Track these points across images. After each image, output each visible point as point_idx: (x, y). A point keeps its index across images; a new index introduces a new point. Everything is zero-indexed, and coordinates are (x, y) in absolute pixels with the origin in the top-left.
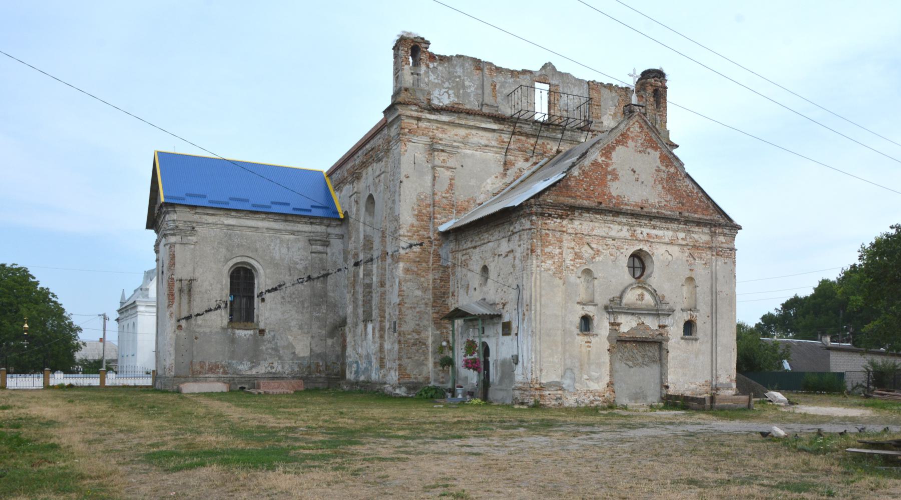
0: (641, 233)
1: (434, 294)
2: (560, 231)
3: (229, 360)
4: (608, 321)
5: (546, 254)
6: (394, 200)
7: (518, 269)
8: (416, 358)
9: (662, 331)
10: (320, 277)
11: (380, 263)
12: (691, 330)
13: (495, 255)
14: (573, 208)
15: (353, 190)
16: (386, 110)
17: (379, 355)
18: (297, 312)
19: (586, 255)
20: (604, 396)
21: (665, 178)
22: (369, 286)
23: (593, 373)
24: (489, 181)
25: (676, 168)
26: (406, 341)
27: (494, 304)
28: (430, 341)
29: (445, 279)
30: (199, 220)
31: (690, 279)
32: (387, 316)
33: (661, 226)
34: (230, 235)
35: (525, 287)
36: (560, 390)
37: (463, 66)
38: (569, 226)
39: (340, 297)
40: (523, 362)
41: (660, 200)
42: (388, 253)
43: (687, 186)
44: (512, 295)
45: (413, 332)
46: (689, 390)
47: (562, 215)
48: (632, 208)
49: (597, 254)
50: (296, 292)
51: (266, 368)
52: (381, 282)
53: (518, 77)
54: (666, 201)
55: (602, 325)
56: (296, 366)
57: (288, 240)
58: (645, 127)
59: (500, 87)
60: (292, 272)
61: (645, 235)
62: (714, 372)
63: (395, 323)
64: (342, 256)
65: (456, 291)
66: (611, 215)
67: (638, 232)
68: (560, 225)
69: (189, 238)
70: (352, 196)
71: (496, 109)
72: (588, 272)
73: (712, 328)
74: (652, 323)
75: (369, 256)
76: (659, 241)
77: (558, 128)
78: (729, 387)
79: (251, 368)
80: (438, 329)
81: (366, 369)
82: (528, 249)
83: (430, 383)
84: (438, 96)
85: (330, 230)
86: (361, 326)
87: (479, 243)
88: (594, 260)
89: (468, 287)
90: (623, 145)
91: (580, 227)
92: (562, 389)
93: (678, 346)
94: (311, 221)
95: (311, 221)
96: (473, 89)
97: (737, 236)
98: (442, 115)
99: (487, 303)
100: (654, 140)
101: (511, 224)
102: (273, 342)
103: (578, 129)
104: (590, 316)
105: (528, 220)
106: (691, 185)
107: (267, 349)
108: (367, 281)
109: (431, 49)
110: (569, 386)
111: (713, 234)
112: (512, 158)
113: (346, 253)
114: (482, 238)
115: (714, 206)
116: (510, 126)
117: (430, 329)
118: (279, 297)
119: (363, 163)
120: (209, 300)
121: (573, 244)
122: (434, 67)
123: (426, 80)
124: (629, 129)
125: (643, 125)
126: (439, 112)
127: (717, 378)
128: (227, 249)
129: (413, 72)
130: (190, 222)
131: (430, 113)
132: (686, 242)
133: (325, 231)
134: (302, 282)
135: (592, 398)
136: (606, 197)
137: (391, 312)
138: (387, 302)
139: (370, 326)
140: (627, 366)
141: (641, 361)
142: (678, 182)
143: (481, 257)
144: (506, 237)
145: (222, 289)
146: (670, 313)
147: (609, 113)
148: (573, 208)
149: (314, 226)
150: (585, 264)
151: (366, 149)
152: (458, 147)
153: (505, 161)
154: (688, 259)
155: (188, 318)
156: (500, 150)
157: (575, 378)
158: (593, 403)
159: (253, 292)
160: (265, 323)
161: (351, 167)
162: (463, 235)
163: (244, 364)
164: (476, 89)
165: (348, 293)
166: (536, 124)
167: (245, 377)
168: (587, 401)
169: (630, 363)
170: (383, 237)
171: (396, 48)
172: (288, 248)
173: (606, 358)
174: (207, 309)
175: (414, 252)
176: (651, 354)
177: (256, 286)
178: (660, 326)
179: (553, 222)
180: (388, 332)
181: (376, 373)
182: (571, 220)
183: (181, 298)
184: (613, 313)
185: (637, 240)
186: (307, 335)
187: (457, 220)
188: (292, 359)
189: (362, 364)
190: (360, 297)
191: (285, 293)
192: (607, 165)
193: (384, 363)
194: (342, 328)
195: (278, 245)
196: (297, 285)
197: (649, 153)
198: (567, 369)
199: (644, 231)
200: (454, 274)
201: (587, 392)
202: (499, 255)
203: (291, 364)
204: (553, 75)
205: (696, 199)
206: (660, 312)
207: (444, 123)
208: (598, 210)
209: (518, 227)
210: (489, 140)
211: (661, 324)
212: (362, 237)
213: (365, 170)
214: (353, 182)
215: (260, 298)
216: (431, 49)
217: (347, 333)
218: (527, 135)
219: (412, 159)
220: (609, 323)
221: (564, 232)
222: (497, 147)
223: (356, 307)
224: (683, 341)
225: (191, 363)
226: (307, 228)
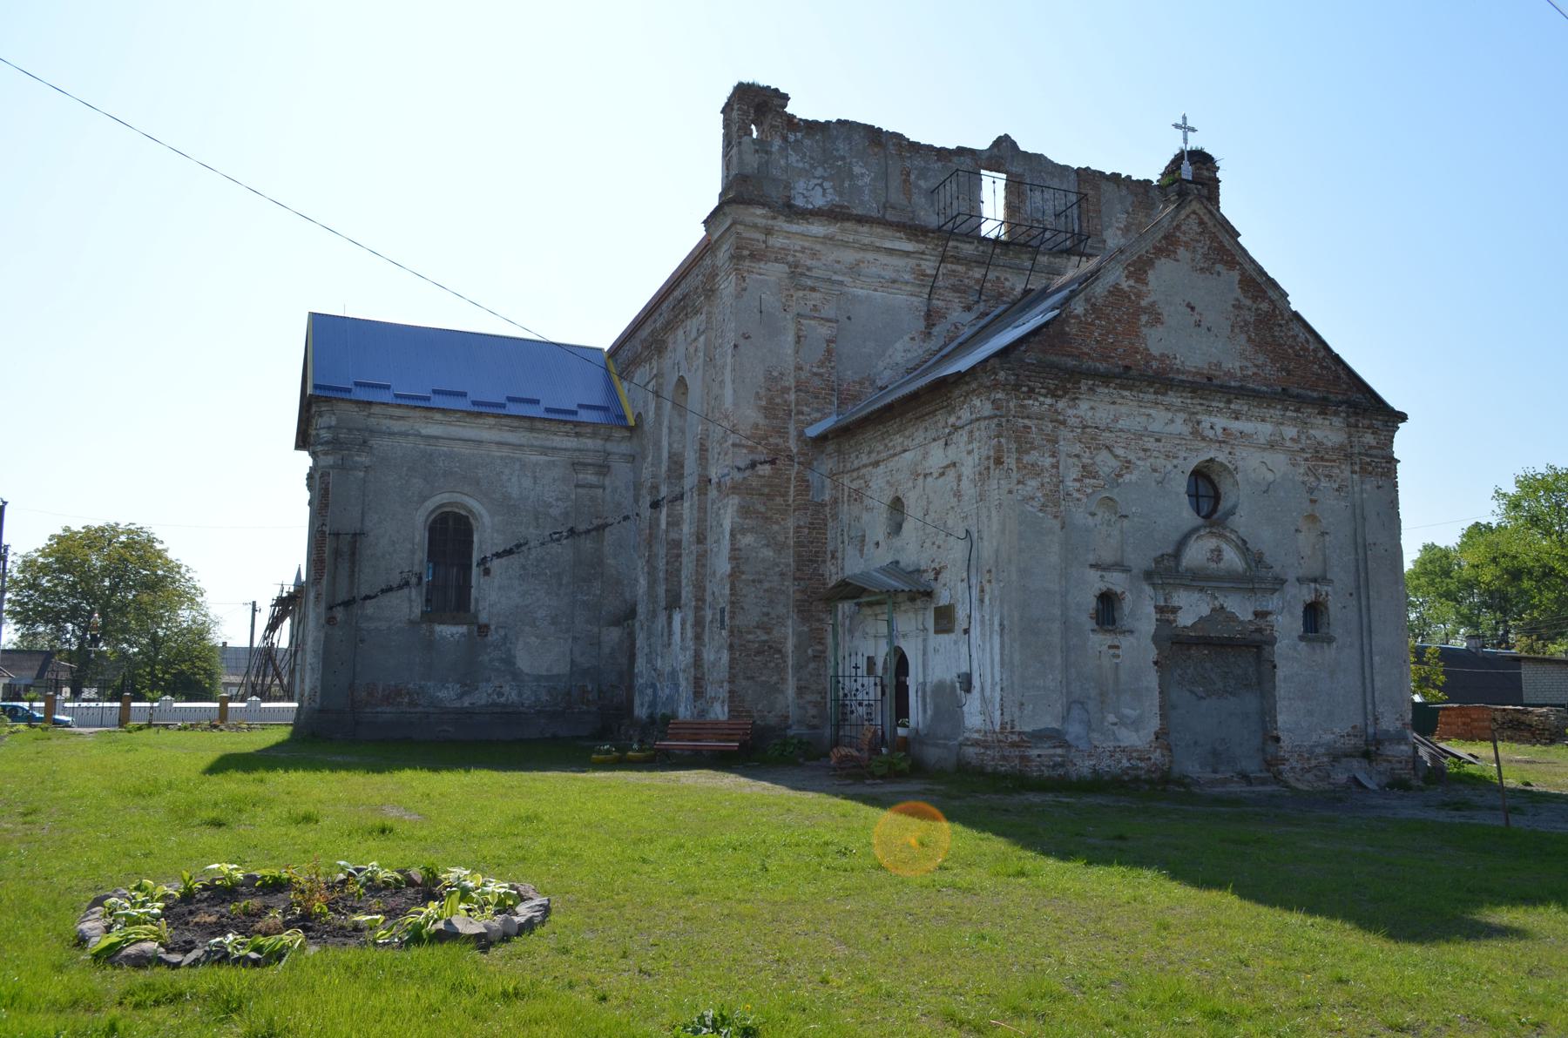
0: (1212, 428)
1: (799, 555)
4: (1153, 603)
8: (763, 678)
9: (1262, 623)
10: (593, 530)
12: (1113, 607)
13: (918, 475)
15: (650, 372)
16: (708, 217)
19: (1104, 471)
20: (1150, 759)
22: (677, 544)
23: (1127, 711)
24: (898, 345)
26: (744, 645)
32: (709, 598)
36: (1061, 747)
38: (1070, 412)
40: (982, 689)
42: (710, 480)
43: (1295, 337)
45: (758, 627)
46: (1322, 745)
49: (1127, 468)
50: (548, 557)
51: (489, 695)
53: (950, 161)
54: (1256, 366)
55: (1141, 612)
57: (536, 464)
61: (1219, 431)
62: (1370, 707)
63: (723, 611)
64: (632, 492)
66: (1152, 390)
73: (1361, 616)
75: (677, 490)
77: (1024, 249)
79: (460, 697)
81: (670, 698)
83: (789, 727)
84: (805, 192)
85: (610, 446)
87: (884, 455)
88: (1120, 480)
90: (1168, 256)
91: (1090, 414)
92: (1065, 744)
95: (578, 430)
96: (867, 180)
98: (813, 224)
101: (951, 411)
102: (503, 648)
104: (1116, 594)
112: (940, 304)
113: (637, 486)
114: (890, 445)
117: (790, 622)
119: (668, 323)
121: (1077, 448)
122: (796, 141)
123: (782, 162)
124: (1178, 227)
129: (757, 147)
134: (558, 540)
137: (719, 591)
142: (1278, 329)
143: (888, 482)
144: (939, 438)
145: (413, 552)
152: (841, 283)
153: (929, 310)
155: (347, 604)
156: (918, 290)
157: (1089, 721)
165: (640, 557)
172: (535, 478)
173: (1152, 679)
174: (384, 587)
175: (760, 476)
177: (476, 546)
178: (1256, 614)
179: (1037, 403)
180: (710, 628)
181: (686, 707)
183: (336, 568)
186: (566, 636)
189: (662, 689)
190: (661, 564)
192: (1139, 296)
193: (701, 687)
194: (630, 622)
197: (1219, 274)
198: (1074, 702)
200: (835, 516)
201: (1115, 751)
202: (925, 476)
203: (534, 688)
204: (1012, 156)
210: (898, 271)
211: (1259, 609)
212: (665, 455)
217: (637, 631)
219: (757, 304)
220: (1156, 607)
223: (652, 583)
226: (571, 443)
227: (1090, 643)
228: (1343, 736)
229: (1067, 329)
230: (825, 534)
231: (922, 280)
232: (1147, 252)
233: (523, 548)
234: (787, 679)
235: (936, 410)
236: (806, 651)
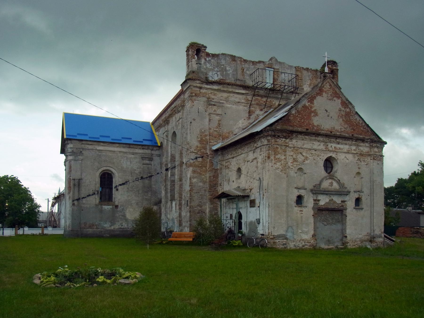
0: (331, 147)
2: (285, 146)
4: (312, 198)
5: (276, 159)
6: (187, 133)
7: (259, 168)
9: (343, 204)
11: (179, 168)
14: (292, 132)
15: (165, 130)
17: (179, 219)
20: (310, 242)
21: (344, 114)
22: (173, 181)
23: (304, 229)
24: (240, 122)
25: (350, 109)
27: (244, 190)
28: (208, 211)
29: (216, 176)
30: (84, 148)
31: (358, 173)
32: (183, 197)
33: (342, 142)
34: (100, 155)
35: (264, 179)
36: (285, 239)
37: (225, 59)
38: (290, 143)
39: (159, 188)
40: (263, 223)
41: (341, 127)
42: (183, 163)
43: (356, 119)
44: (256, 184)
45: (198, 206)
46: (358, 239)
47: (286, 136)
48: (325, 132)
49: (306, 159)
50: (135, 185)
51: (119, 226)
52: (180, 179)
53: (256, 65)
54: (345, 128)
57: (131, 158)
58: (333, 85)
59: (247, 70)
60: (133, 175)
61: (333, 148)
63: (187, 201)
64: (160, 166)
65: (222, 183)
66: (314, 136)
67: (329, 146)
68: (285, 142)
69: (79, 157)
70: (164, 133)
71: (244, 82)
72: (300, 169)
74: (338, 200)
75: (173, 165)
76: (341, 151)
77: (279, 92)
78: (380, 237)
79: (111, 226)
82: (266, 157)
84: (212, 76)
85: (153, 152)
86: (169, 203)
87: (235, 155)
88: (304, 163)
89: (229, 180)
90: (320, 95)
91: (296, 143)
92: (286, 239)
93: (352, 213)
96: (231, 71)
97: (384, 148)
98: (214, 85)
99: (241, 189)
100: (338, 92)
102: (122, 212)
103: (290, 92)
105: (266, 139)
106: (358, 119)
108: (172, 179)
109: (207, 50)
110: (290, 237)
111: (371, 147)
112: (253, 109)
113: (161, 164)
114: (237, 152)
115: (371, 131)
116: (252, 91)
117: (207, 204)
121: (292, 153)
122: (209, 60)
123: (205, 67)
125: (331, 84)
126: (212, 84)
127: (374, 231)
128: (99, 163)
129: (197, 62)
130: (79, 148)
131: (207, 85)
132: (356, 152)
133: (150, 153)
135: (303, 244)
136: (311, 126)
137: (186, 195)
138: (183, 190)
139: (174, 203)
140: (323, 225)
141: (331, 221)
142: (352, 117)
144: (252, 151)
145: (96, 184)
146: (348, 193)
147: (307, 84)
148: (292, 132)
149: (145, 150)
151: (172, 108)
152: (223, 103)
153: (249, 111)
154: (358, 162)
155: (78, 200)
156: (247, 105)
157: (294, 232)
158: (304, 247)
159: (112, 185)
160: (118, 202)
161: (164, 118)
162: (226, 151)
163: (107, 224)
164: (233, 71)
166: (267, 90)
167: (107, 231)
168: (301, 246)
169: (325, 223)
170: (181, 154)
171: (187, 51)
173: (312, 220)
174: (88, 195)
176: (336, 218)
177: (114, 182)
179: (280, 140)
184: (316, 193)
185: (329, 151)
187: (223, 143)
189: (170, 224)
190: (169, 187)
192: (311, 107)
194: (160, 204)
195: (125, 160)
198: (289, 227)
199: (332, 145)
200: (221, 173)
202: (248, 161)
204: (276, 64)
205: (361, 127)
207: (215, 90)
209: (259, 144)
212: (170, 155)
213: (172, 119)
214: (165, 126)
215: (116, 189)
216: (207, 50)
218: (262, 96)
219: (197, 110)
220: (313, 200)
221: (287, 146)
222: (245, 103)
223: (166, 193)
224: (355, 210)
225: (80, 223)
228: (364, 236)
229: (290, 118)
231: (248, 102)
232: (314, 94)
233: (128, 183)
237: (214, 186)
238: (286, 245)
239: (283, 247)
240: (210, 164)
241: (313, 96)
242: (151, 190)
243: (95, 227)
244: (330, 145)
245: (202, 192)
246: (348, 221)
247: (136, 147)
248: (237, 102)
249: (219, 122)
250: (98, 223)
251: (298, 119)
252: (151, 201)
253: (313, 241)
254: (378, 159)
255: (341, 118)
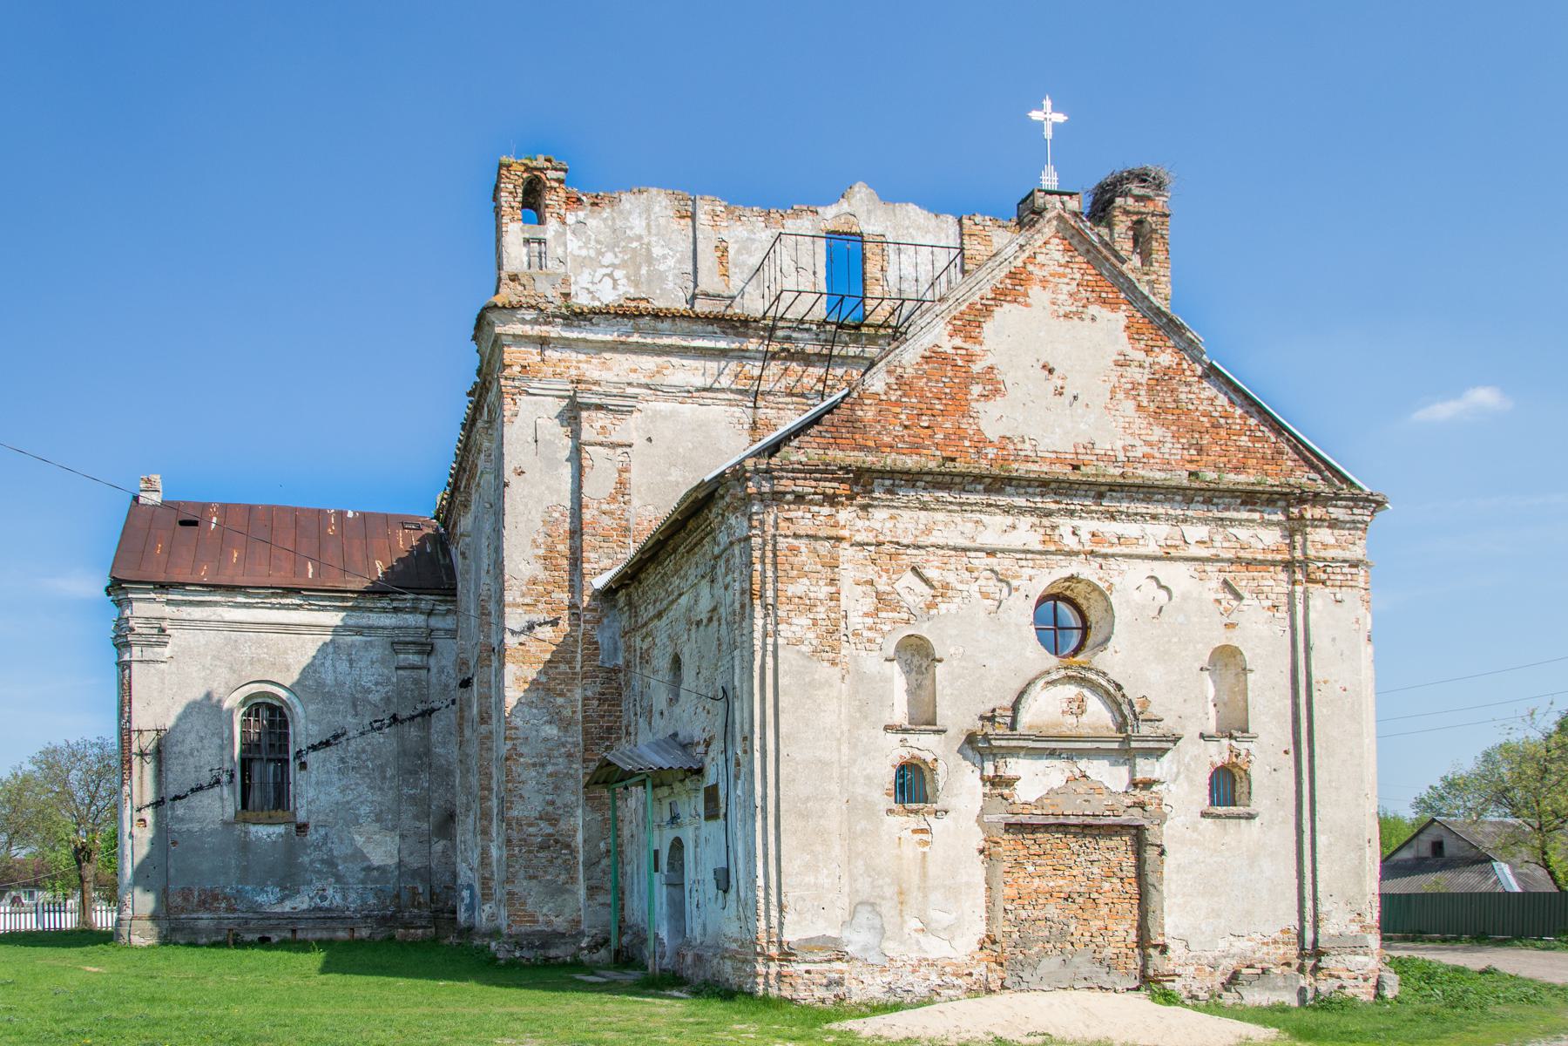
1: (586, 732)
2: (828, 538)
3: (237, 883)
8: (549, 877)
10: (418, 716)
18: (370, 787)
21: (1144, 381)
26: (525, 840)
34: (236, 641)
38: (860, 524)
41: (1130, 440)
43: (1212, 400)
45: (541, 818)
50: (368, 748)
51: (311, 899)
56: (371, 896)
57: (352, 645)
59: (738, 252)
60: (359, 708)
61: (1086, 537)
66: (980, 487)
74: (1111, 776)
77: (882, 331)
78: (1358, 948)
79: (281, 901)
80: (594, 809)
84: (590, 286)
85: (435, 622)
91: (889, 524)
93: (1195, 835)
94: (395, 604)
95: (395, 604)
96: (671, 262)
102: (324, 849)
105: (744, 515)
107: (312, 862)
110: (865, 949)
118: (335, 759)
120: (198, 768)
121: (870, 572)
128: (231, 668)
129: (527, 236)
132: (1213, 551)
133: (423, 624)
136: (967, 443)
142: (1187, 389)
150: (908, 622)
157: (882, 927)
160: (309, 812)
167: (269, 918)
172: (351, 662)
173: (976, 871)
177: (291, 738)
182: (864, 508)
188: (363, 882)
191: (346, 751)
192: (970, 358)
193: (490, 888)
195: (330, 657)
196: (370, 735)
197: (1093, 319)
198: (861, 903)
200: (628, 683)
203: (360, 891)
206: (1133, 745)
208: (945, 480)
211: (1139, 777)
218: (806, 359)
220: (982, 778)
221: (839, 539)
226: (388, 620)
227: (885, 827)
228: (1267, 944)
229: (860, 413)
230: (619, 705)
233: (342, 739)
234: (577, 878)
235: (703, 538)
236: (597, 846)
237: (602, 738)
238: (842, 985)
239: (828, 995)
240: (588, 649)
241: (979, 306)
242: (430, 766)
243: (223, 905)
244: (1065, 525)
245: (557, 764)
246: (1174, 877)
247: (368, 605)
248: (698, 390)
249: (620, 476)
250: (232, 888)
251: (903, 417)
252: (429, 807)
253: (982, 969)
254: (1339, 577)
255: (1127, 398)
